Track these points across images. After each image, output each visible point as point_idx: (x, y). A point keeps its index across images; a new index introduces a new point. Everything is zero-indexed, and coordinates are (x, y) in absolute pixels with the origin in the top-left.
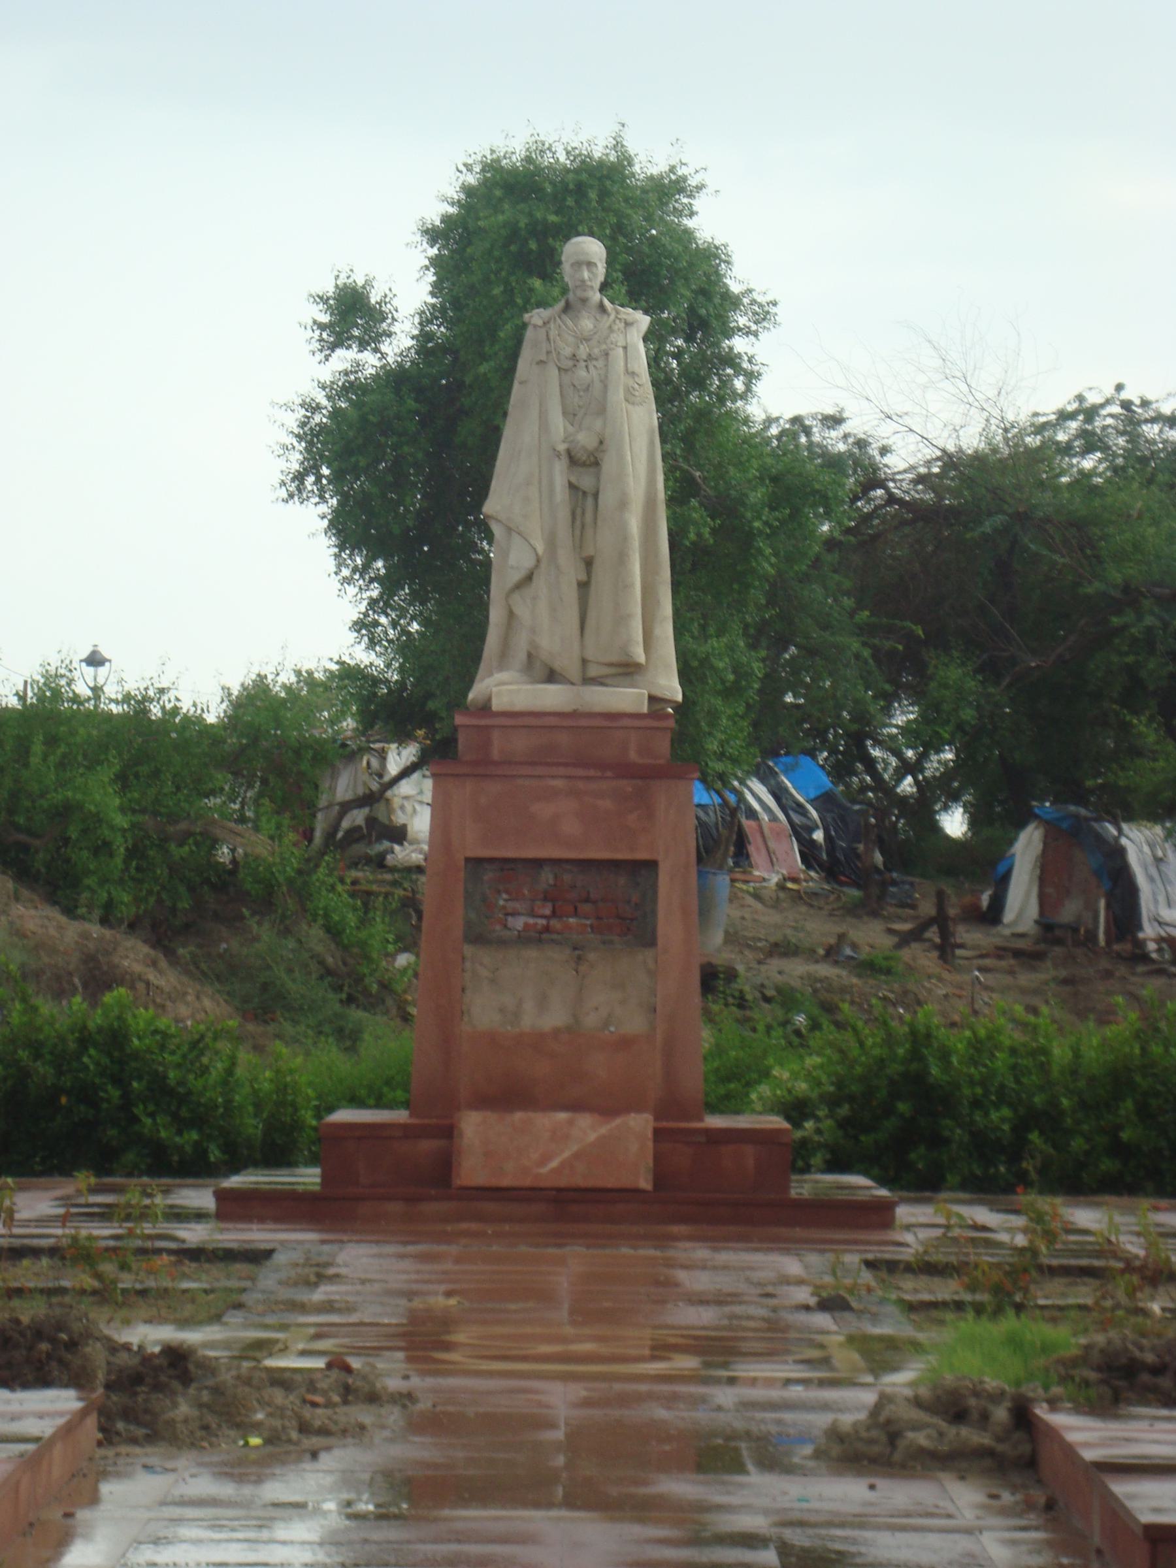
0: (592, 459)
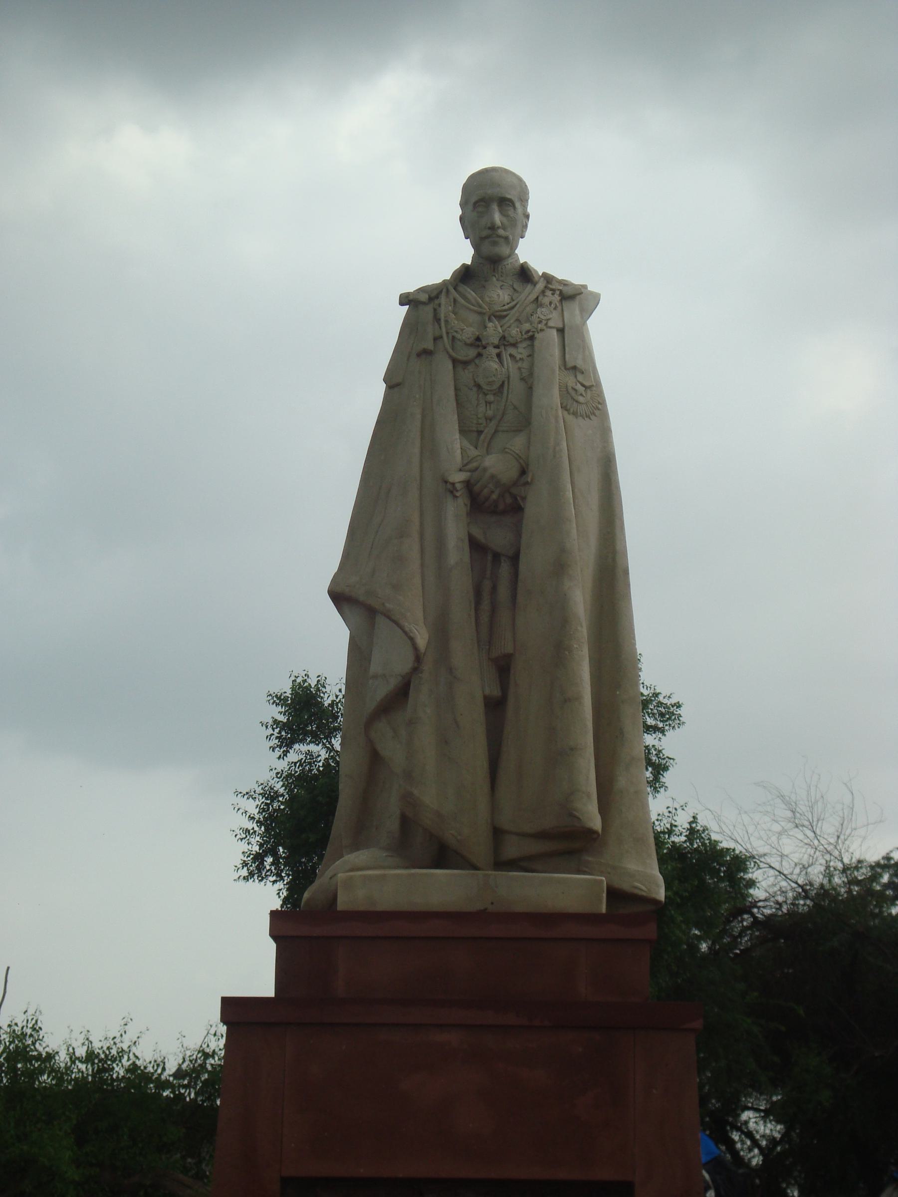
0: (509, 500)
